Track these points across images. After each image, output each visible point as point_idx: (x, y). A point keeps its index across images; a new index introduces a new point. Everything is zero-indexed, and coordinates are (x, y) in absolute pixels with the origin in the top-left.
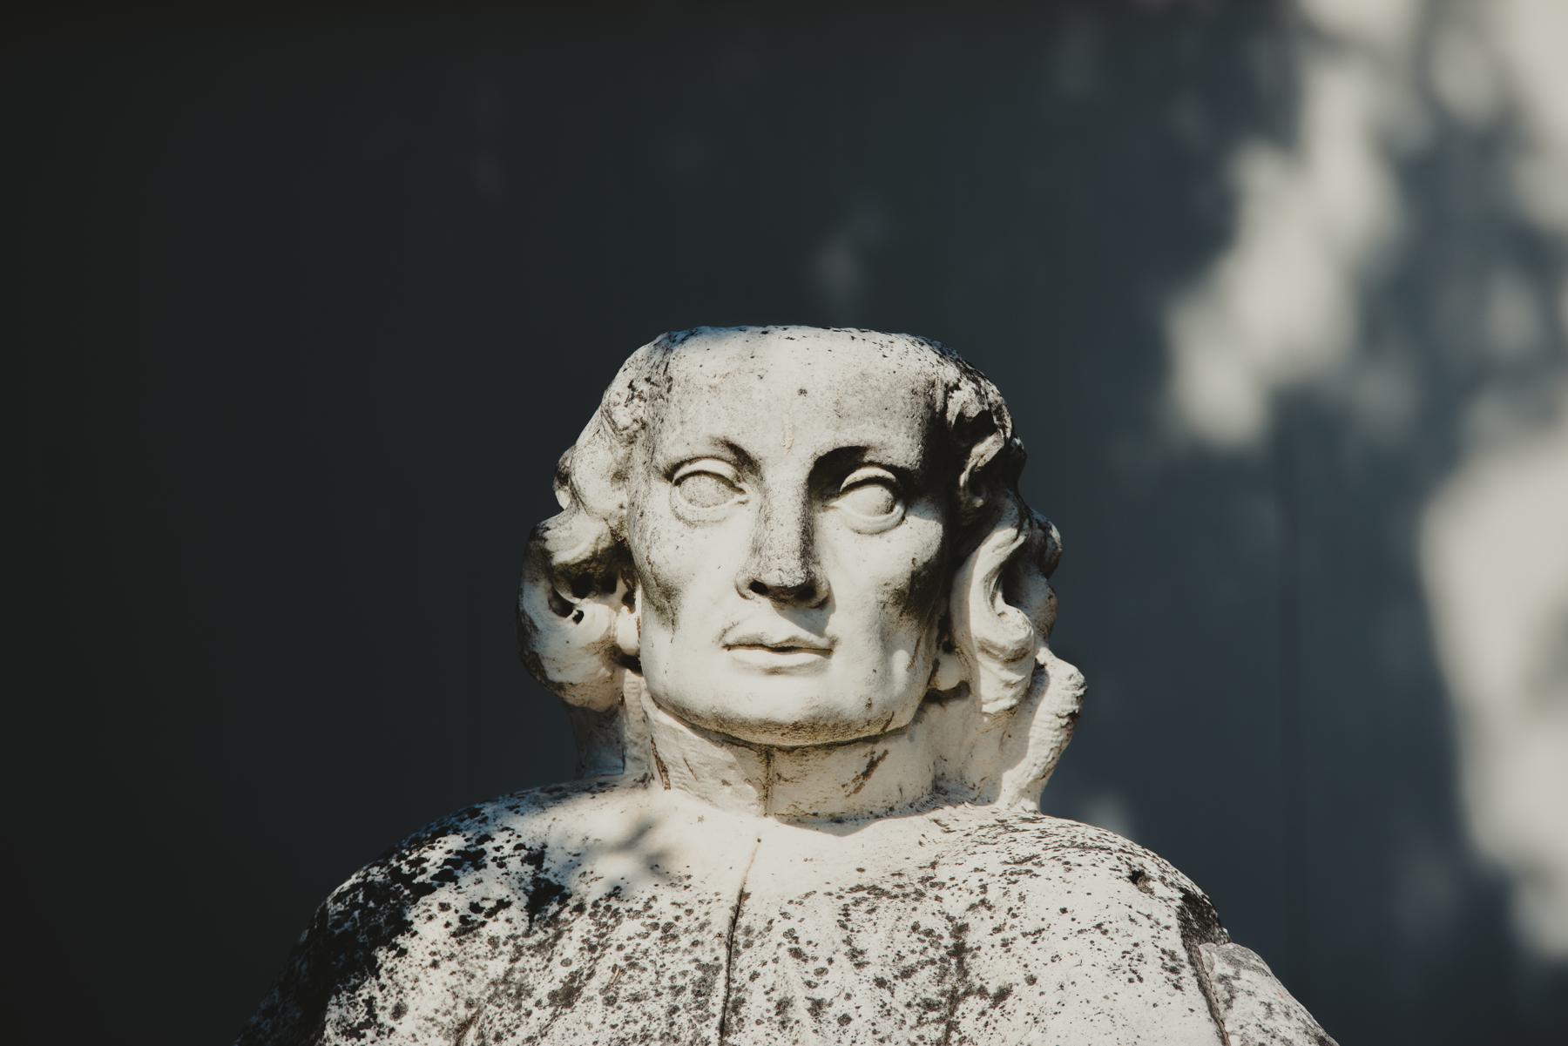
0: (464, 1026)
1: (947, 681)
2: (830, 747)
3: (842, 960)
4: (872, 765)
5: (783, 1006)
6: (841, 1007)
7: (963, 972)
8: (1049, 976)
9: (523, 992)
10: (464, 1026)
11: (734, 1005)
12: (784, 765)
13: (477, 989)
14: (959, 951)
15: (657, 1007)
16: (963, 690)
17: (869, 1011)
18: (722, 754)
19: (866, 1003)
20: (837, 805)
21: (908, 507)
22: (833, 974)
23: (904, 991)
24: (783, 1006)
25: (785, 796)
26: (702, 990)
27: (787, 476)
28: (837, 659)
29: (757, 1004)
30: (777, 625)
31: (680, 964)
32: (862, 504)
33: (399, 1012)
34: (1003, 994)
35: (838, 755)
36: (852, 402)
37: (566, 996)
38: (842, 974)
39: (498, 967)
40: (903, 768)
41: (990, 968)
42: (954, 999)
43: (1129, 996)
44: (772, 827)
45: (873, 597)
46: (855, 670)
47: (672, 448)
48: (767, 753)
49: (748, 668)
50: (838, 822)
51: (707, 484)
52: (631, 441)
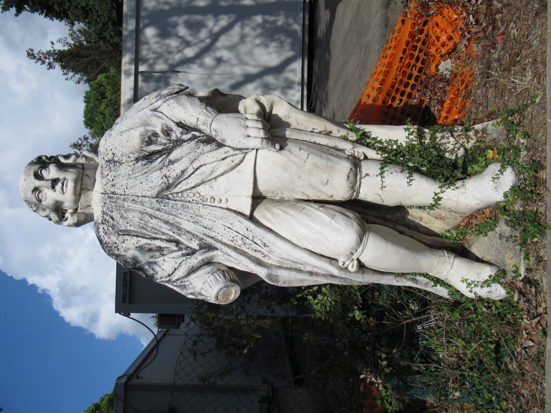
0: (119, 234)
1: (81, 167)
2: (82, 180)
3: (107, 177)
4: (87, 175)
5: (113, 186)
6: (113, 177)
7: (111, 160)
8: (111, 147)
9: (113, 225)
10: (119, 234)
11: (113, 193)
12: (84, 187)
13: (113, 232)
14: (109, 161)
15: (113, 204)
16: (82, 164)
17: (114, 173)
18: (83, 196)
19: (113, 173)
20: (93, 181)
21: (48, 167)
22: (109, 178)
23: (112, 168)
24: (113, 186)
25: (89, 187)
26: (110, 198)
27: (38, 183)
28: (67, 178)
29: (112, 190)
30: (58, 187)
31: (108, 201)
32: (44, 173)
33: (116, 243)
34: (113, 154)
35: (83, 179)
36: (27, 173)
37: (112, 218)
38: (109, 177)
39: (111, 229)
40: (145, 211)
41: (110, 156)
42: (114, 161)
43: (113, 136)
44: (95, 190)
45: (59, 172)
46: (70, 177)
47: (35, 200)
48: (82, 189)
49: (66, 190)
50: (95, 181)
51: (40, 195)
52: (38, 208)
